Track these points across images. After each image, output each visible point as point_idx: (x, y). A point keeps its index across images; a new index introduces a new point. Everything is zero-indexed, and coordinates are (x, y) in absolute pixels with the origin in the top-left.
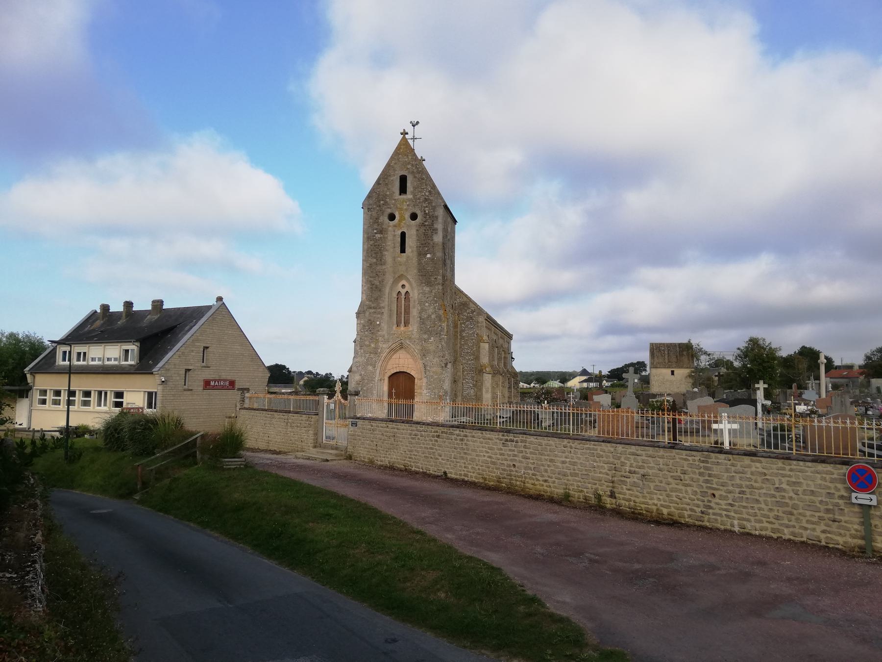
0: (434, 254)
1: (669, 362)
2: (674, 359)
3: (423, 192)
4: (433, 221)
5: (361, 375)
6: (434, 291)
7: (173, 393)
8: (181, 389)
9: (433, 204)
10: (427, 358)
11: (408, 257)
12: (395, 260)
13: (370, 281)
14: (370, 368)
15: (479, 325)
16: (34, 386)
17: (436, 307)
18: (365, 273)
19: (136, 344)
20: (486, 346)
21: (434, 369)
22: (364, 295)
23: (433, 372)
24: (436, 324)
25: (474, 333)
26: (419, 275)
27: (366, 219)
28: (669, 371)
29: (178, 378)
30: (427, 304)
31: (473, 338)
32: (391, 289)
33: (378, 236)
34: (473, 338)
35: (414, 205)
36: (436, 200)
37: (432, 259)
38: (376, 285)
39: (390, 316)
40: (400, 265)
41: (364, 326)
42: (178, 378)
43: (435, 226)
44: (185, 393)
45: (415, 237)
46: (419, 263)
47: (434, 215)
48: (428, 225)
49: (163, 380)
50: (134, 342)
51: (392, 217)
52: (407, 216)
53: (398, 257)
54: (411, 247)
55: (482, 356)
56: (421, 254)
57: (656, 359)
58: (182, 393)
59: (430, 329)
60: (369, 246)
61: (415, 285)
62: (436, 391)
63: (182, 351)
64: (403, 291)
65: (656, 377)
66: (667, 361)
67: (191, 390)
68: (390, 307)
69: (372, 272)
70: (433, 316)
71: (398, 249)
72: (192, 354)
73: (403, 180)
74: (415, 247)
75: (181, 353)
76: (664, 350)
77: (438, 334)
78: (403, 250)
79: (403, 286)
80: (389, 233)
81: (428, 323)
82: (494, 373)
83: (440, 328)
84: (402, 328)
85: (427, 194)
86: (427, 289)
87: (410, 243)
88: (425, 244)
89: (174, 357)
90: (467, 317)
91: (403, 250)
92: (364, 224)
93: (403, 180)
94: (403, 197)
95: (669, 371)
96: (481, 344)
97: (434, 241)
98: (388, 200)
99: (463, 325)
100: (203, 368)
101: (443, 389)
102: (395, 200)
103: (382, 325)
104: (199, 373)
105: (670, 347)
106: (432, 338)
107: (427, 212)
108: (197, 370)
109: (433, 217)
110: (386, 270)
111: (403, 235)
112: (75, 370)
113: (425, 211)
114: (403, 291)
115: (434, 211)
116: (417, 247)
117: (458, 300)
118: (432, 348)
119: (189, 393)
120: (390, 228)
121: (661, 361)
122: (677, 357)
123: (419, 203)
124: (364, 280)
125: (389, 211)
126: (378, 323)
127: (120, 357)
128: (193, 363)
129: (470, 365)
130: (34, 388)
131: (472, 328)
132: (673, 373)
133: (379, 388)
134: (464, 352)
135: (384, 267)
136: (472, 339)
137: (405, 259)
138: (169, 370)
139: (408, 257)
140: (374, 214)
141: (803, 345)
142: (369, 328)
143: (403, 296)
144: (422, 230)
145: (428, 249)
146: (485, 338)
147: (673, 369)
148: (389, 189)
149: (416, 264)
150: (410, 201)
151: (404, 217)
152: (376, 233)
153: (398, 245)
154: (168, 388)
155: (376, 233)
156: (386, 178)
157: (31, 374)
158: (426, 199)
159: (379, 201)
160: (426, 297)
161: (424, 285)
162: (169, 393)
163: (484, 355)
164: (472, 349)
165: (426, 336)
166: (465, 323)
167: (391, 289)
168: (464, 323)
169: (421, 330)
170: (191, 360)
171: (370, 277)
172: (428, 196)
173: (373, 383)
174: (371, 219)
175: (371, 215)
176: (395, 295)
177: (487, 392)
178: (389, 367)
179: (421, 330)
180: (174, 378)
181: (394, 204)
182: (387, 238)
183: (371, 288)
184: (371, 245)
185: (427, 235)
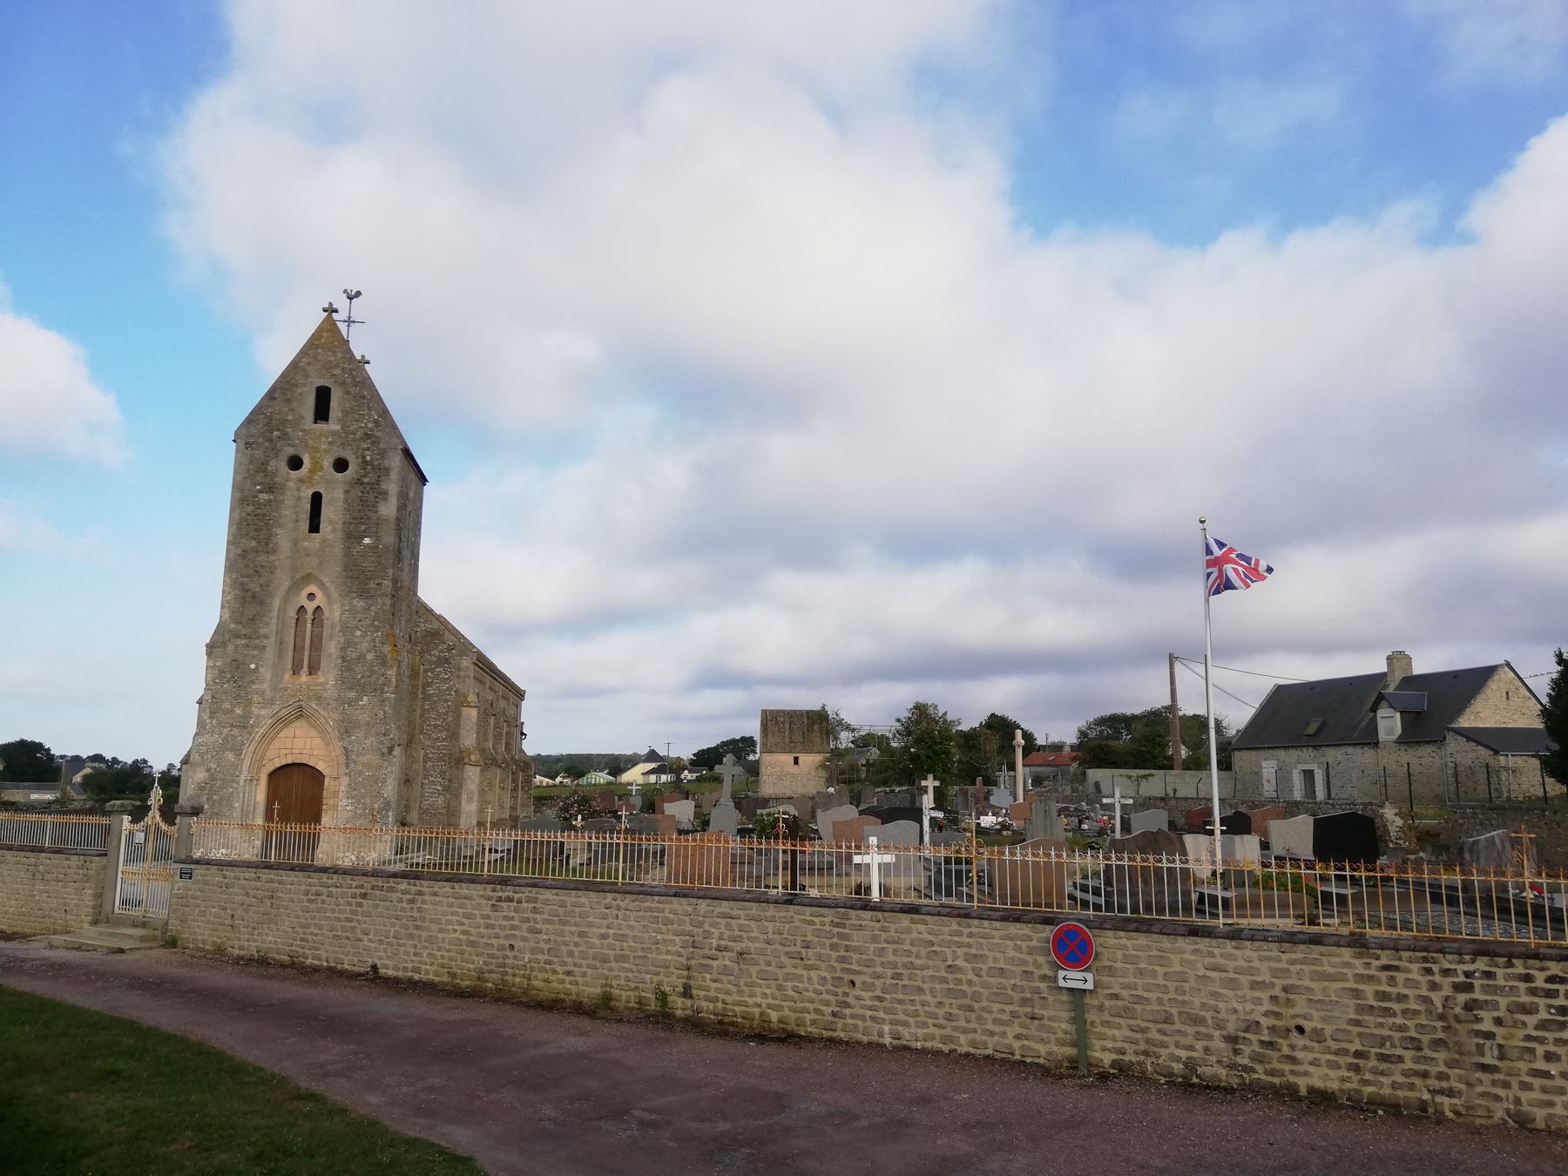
0: (377, 537)
1: (791, 742)
3: (362, 422)
5: (208, 770)
12: (296, 545)
13: (242, 584)
14: (230, 756)
15: (462, 673)
18: (230, 567)
20: (474, 713)
22: (226, 610)
25: (449, 689)
26: (346, 577)
28: (790, 758)
30: (358, 633)
32: (286, 600)
33: (264, 497)
34: (448, 697)
37: (373, 547)
39: (280, 654)
40: (306, 555)
41: (222, 672)
43: (384, 486)
48: (368, 484)
51: (296, 463)
52: (327, 463)
55: (463, 732)
56: (352, 537)
57: (770, 737)
60: (244, 515)
61: (336, 595)
62: (368, 801)
64: (310, 607)
66: (787, 740)
70: (370, 656)
71: (305, 525)
73: (323, 396)
77: (378, 690)
78: (314, 527)
84: (304, 677)
86: (360, 604)
87: (332, 514)
88: (362, 518)
90: (439, 657)
91: (314, 527)
92: (236, 472)
93: (323, 396)
94: (321, 426)
95: (790, 758)
96: (464, 709)
102: (304, 431)
103: (262, 670)
105: (793, 716)
106: (365, 698)
107: (368, 458)
110: (276, 563)
111: (317, 499)
113: (364, 457)
114: (310, 607)
115: (382, 458)
116: (344, 523)
121: (778, 740)
122: (803, 734)
125: (290, 451)
126: (253, 666)
131: (447, 679)
132: (796, 761)
134: (428, 726)
135: (272, 558)
136: (447, 701)
139: (325, 541)
140: (259, 454)
145: (366, 529)
146: (472, 698)
147: (796, 755)
152: (260, 492)
155: (260, 492)
156: (287, 389)
161: (354, 595)
164: (445, 720)
165: (352, 695)
167: (286, 600)
168: (432, 670)
172: (371, 430)
173: (235, 785)
174: (251, 462)
177: (470, 800)
178: (270, 754)
183: (243, 597)
185: (366, 501)
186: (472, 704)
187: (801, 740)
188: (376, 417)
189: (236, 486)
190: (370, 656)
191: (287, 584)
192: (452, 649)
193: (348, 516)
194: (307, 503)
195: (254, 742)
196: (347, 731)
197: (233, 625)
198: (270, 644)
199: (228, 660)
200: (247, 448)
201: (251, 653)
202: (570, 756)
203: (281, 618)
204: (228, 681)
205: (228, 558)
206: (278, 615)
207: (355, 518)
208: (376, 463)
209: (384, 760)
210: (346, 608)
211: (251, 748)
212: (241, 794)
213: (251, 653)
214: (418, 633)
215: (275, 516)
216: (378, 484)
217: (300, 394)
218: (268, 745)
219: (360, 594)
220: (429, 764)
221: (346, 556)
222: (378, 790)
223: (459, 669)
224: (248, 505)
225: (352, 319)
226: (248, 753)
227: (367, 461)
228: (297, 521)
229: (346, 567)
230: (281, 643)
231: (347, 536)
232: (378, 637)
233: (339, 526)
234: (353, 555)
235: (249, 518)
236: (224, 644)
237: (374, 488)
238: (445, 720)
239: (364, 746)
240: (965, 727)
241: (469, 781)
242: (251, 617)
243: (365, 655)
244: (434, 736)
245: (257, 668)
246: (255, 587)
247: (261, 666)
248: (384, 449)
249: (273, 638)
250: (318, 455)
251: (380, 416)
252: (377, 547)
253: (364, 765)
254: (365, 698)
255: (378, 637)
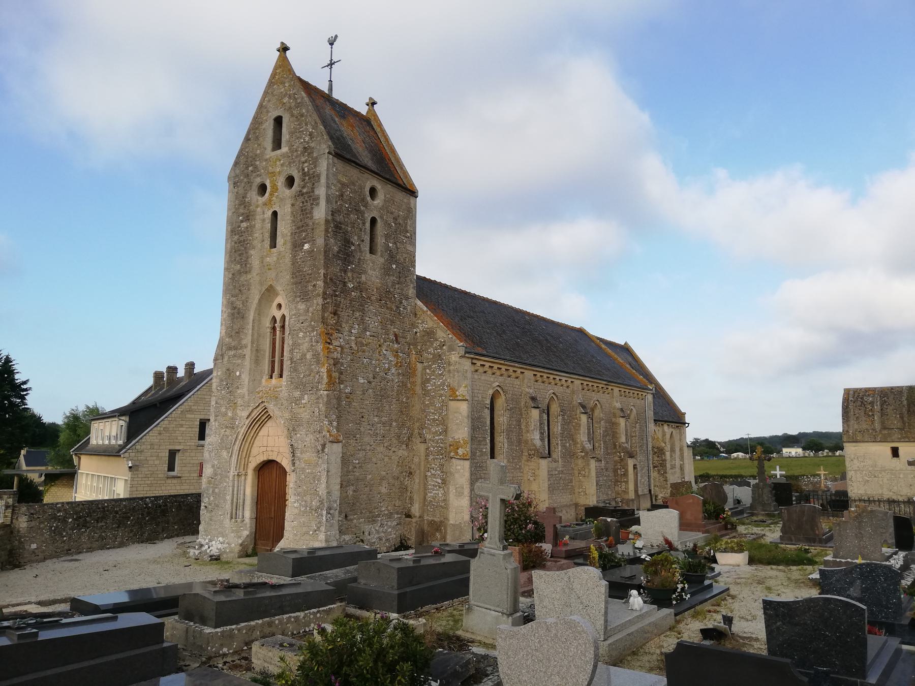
0: (313, 242)
1: (885, 428)
2: (895, 422)
3: (301, 138)
4: (313, 184)
5: (213, 466)
6: (311, 309)
7: (149, 482)
8: (162, 476)
9: (315, 155)
10: (298, 435)
11: (280, 253)
12: (263, 263)
13: (232, 303)
14: (224, 454)
15: (452, 368)
16: (79, 469)
17: (314, 338)
18: (226, 291)
19: (123, 418)
20: (464, 407)
21: (306, 456)
22: (223, 327)
23: (305, 462)
24: (312, 371)
25: (443, 384)
27: (231, 201)
28: (884, 449)
29: (157, 462)
30: (301, 334)
31: (442, 392)
32: (260, 312)
33: (244, 225)
34: (442, 392)
35: (290, 163)
36: (318, 147)
37: (310, 252)
38: (239, 309)
39: (257, 361)
41: (222, 380)
42: (157, 462)
43: (317, 192)
44: (169, 481)
45: (289, 218)
46: (294, 262)
47: (316, 173)
48: (307, 193)
49: (130, 465)
50: (118, 416)
51: (263, 189)
52: (281, 181)
53: (266, 257)
54: (283, 236)
55: (452, 426)
56: (297, 246)
57: (852, 422)
58: (163, 482)
59: (304, 380)
60: (233, 243)
62: (308, 498)
63: (164, 426)
65: (855, 461)
66: (877, 426)
67: (180, 477)
68: (257, 346)
69: (235, 287)
70: (309, 356)
71: (267, 243)
72: (181, 429)
74: (289, 234)
75: (162, 429)
76: (872, 403)
77: (315, 388)
79: (279, 306)
80: (258, 217)
81: (302, 368)
82: (530, 455)
83: (317, 376)
84: (274, 381)
85: (307, 139)
86: (302, 306)
87: (284, 228)
88: (303, 226)
89: (150, 434)
90: (434, 355)
91: (273, 245)
92: (229, 209)
93: (278, 121)
94: (278, 152)
95: (884, 449)
97: (314, 218)
98: (258, 163)
99: (428, 371)
100: (199, 448)
101: (318, 495)
102: (266, 160)
103: (243, 376)
104: (192, 454)
105: (887, 395)
106: (306, 396)
107: (306, 169)
108: (189, 451)
109: (314, 176)
110: (251, 281)
111: (275, 214)
112: (95, 452)
113: (304, 170)
115: (315, 167)
116: (292, 233)
117: (420, 326)
118: (305, 415)
119: (175, 481)
120: (259, 209)
121: (864, 426)
122: (902, 417)
123: (297, 157)
124: (225, 303)
125: (258, 180)
127: (117, 435)
128: (182, 441)
129: (437, 442)
130: (79, 471)
131: (441, 375)
132: (895, 452)
133: (235, 489)
134: (428, 420)
135: (249, 276)
136: (441, 396)
137: (275, 259)
138: (141, 452)
139: (280, 253)
140: (241, 191)
141: (154, 372)
142: (227, 384)
143: (278, 325)
144: (299, 203)
145: (306, 236)
146: (462, 391)
148: (260, 145)
149: (289, 264)
150: (284, 157)
151: (277, 186)
153: (267, 235)
154: (140, 476)
155: (242, 222)
156: (257, 129)
157: (76, 454)
158: (305, 148)
159: (247, 168)
160: (301, 321)
161: (298, 299)
162: (143, 482)
163: (457, 424)
164: (440, 414)
165: (297, 394)
166: (431, 366)
167: (260, 312)
168: (429, 367)
169: (292, 383)
170: (179, 438)
171: (232, 296)
172: (308, 143)
174: (236, 198)
175: (237, 193)
176: (267, 323)
177: (460, 494)
178: (255, 451)
179: (292, 383)
180: (150, 462)
181: (265, 168)
182: (255, 225)
184: (236, 243)
185: (305, 210)
186: (460, 398)
187: (900, 425)
188: (311, 130)
189: (230, 222)
190: (309, 356)
191: (257, 297)
192: (443, 345)
193: (294, 227)
194: (268, 223)
195: (238, 441)
196: (294, 430)
197: (227, 340)
198: (247, 352)
199: (224, 369)
200: (234, 187)
201: (237, 362)
202: (730, 441)
203: (256, 328)
204: (224, 388)
205: (224, 284)
206: (253, 326)
207: (298, 228)
208: (311, 172)
209: (319, 458)
210: (293, 313)
211: (236, 446)
212: (231, 488)
213: (237, 362)
214: (418, 334)
215: (250, 240)
216: (313, 192)
217: (264, 129)
218: (251, 444)
219: (302, 297)
220: (431, 457)
221: (293, 264)
222: (315, 488)
223: (449, 364)
224: (235, 235)
225: (333, 61)
226: (235, 451)
227: (305, 173)
228: (263, 241)
229: (293, 275)
230: (258, 351)
231: (293, 245)
232: (314, 336)
233: (289, 238)
234: (298, 263)
235: (236, 245)
236: (222, 355)
237: (311, 196)
238: (440, 414)
239: (305, 443)
240: (44, 421)
241: (457, 475)
242: (237, 331)
243: (305, 355)
244: (433, 430)
245: (240, 375)
246: (239, 304)
247: (243, 372)
248: (316, 158)
249: (249, 347)
250: (275, 178)
251: (313, 129)
252: (313, 250)
253: (305, 462)
254: (306, 396)
255: (314, 336)
